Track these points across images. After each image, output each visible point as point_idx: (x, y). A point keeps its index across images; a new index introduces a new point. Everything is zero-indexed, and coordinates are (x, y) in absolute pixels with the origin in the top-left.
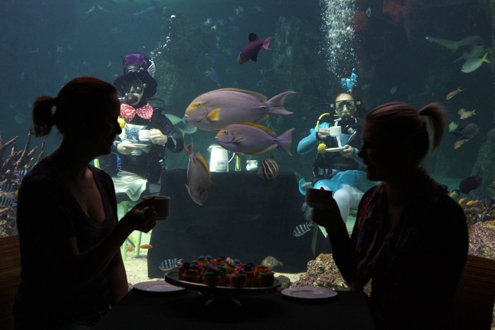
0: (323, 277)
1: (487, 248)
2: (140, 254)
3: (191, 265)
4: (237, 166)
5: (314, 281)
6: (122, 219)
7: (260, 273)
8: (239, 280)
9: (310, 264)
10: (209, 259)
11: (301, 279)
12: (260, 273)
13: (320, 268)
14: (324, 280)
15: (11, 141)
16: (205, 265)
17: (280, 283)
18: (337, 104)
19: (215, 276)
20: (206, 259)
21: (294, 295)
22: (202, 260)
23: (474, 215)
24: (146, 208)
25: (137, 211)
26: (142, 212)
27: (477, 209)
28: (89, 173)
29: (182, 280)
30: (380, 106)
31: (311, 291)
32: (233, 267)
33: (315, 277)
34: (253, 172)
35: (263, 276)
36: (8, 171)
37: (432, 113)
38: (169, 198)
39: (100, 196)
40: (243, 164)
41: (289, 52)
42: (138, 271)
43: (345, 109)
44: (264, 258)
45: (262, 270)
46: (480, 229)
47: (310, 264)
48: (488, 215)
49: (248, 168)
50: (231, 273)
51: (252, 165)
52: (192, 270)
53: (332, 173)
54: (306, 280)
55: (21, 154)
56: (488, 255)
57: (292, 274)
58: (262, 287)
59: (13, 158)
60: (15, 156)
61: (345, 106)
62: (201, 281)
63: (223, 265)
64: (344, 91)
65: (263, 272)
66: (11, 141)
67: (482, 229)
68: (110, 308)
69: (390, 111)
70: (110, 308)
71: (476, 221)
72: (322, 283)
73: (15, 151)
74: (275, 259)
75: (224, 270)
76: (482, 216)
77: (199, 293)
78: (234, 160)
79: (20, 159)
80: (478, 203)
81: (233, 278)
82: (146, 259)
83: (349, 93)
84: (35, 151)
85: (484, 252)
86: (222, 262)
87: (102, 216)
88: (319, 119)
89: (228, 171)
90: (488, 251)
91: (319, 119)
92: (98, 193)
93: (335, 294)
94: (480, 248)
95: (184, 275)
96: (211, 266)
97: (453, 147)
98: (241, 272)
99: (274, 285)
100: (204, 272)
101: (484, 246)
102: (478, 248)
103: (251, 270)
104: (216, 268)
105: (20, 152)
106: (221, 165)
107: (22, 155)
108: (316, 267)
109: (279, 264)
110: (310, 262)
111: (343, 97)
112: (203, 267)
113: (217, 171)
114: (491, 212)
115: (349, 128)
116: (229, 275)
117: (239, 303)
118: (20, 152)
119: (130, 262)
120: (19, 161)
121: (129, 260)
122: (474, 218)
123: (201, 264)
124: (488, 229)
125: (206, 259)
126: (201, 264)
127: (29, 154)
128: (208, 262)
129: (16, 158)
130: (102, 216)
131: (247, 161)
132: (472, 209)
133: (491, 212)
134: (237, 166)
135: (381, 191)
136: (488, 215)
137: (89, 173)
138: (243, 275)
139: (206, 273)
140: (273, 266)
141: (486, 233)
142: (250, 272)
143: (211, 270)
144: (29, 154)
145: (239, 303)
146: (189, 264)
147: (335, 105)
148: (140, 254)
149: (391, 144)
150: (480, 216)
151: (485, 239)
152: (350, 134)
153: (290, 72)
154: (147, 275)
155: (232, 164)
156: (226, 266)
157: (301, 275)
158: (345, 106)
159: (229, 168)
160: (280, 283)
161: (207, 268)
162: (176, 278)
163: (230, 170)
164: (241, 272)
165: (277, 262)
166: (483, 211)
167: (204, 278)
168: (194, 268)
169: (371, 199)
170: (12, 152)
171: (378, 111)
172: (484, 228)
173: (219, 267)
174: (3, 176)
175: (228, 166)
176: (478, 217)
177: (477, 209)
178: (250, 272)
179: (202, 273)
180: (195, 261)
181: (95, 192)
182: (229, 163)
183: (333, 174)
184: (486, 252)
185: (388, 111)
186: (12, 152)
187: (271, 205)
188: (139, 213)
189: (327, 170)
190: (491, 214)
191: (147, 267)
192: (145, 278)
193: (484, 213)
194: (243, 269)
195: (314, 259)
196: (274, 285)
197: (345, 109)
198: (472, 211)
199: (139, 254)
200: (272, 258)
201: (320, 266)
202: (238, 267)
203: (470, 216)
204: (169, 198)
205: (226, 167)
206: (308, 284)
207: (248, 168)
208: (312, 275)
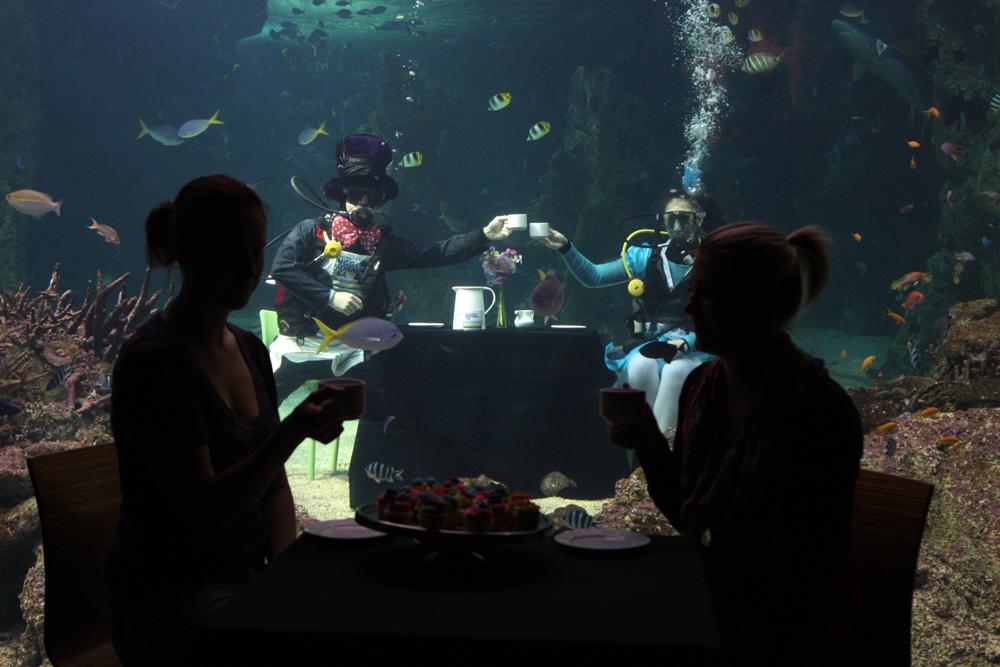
0: (641, 508)
1: (919, 457)
2: (338, 468)
3: (400, 494)
4: (500, 319)
5: (625, 514)
6: (287, 419)
7: (517, 507)
8: (478, 520)
9: (620, 486)
10: (430, 484)
11: (605, 510)
12: (517, 507)
13: (636, 491)
14: (643, 512)
15: (117, 281)
16: (423, 493)
17: (550, 523)
18: (666, 216)
19: (437, 514)
20: (425, 483)
21: (578, 544)
22: (417, 485)
23: (896, 401)
24: (327, 402)
25: (312, 406)
26: (319, 408)
27: (903, 391)
28: (230, 338)
29: (383, 520)
30: (721, 228)
31: (603, 536)
32: (470, 497)
33: (606, 512)
34: (526, 328)
35: (520, 512)
36: (113, 332)
37: (806, 243)
38: (363, 382)
39: (250, 377)
40: (510, 317)
41: (591, 125)
42: (332, 496)
43: (677, 226)
44: (545, 474)
45: (520, 501)
46: (907, 425)
47: (620, 486)
48: (920, 400)
49: (518, 322)
50: (466, 506)
51: (524, 318)
52: (398, 503)
53: (656, 329)
54: (612, 512)
55: (134, 302)
56: (920, 469)
57: (592, 502)
58: (519, 530)
59: (120, 310)
60: (123, 307)
61: (676, 221)
62: (414, 521)
63: (454, 494)
64: (681, 192)
65: (521, 505)
66: (117, 281)
67: (911, 424)
68: (266, 562)
69: (744, 234)
70: (266, 562)
71: (900, 411)
72: (640, 517)
73: (123, 298)
74: (563, 476)
75: (454, 503)
76: (911, 402)
77: (416, 541)
78: (495, 308)
79: (133, 311)
80: (904, 380)
81: (469, 517)
82: (347, 477)
83: (688, 197)
84: (158, 297)
85: (913, 464)
86: (454, 488)
87: (254, 409)
88: (628, 239)
89: (483, 328)
90: (919, 462)
91: (628, 239)
92: (247, 370)
93: (646, 541)
94: (906, 456)
95: (386, 511)
96: (433, 495)
97: (890, 284)
98: (482, 506)
99: (541, 527)
100: (421, 505)
101: (913, 454)
102: (902, 457)
103: (500, 502)
104: (441, 499)
105: (132, 299)
106: (472, 319)
107: (137, 305)
108: (629, 490)
109: (570, 485)
110: (620, 481)
111: (676, 206)
112: (420, 496)
113: (465, 329)
114: (925, 395)
115: (685, 255)
116: (462, 511)
117: (480, 556)
118: (132, 299)
119: (320, 483)
120: (131, 314)
121: (319, 479)
122: (897, 406)
123: (416, 491)
124: (920, 425)
125: (425, 483)
126: (416, 491)
127: (148, 302)
128: (429, 488)
129: (126, 309)
130: (254, 409)
131: (516, 312)
132: (893, 390)
133: (925, 395)
134: (500, 319)
135: (715, 376)
136: (920, 400)
137: (230, 338)
138: (485, 510)
139: (424, 507)
140: (560, 488)
141: (916, 431)
142: (498, 506)
143: (432, 503)
144: (148, 302)
145: (480, 556)
146: (395, 493)
147: (661, 217)
148: (338, 468)
149: (740, 294)
150: (907, 402)
151: (914, 441)
152: (686, 263)
153: (594, 160)
154: (348, 504)
155: (491, 317)
156: (458, 496)
157: (606, 504)
158: (676, 221)
159: (487, 321)
160: (550, 523)
161: (426, 500)
162: (373, 517)
163: (487, 327)
164: (482, 506)
165: (568, 481)
166: (912, 394)
167: (419, 516)
168: (402, 499)
169: (698, 390)
170: (120, 299)
171: (721, 235)
172: (913, 423)
173: (446, 498)
174: (105, 340)
175: (484, 320)
176: (904, 403)
177: (903, 391)
178: (498, 506)
179: (416, 507)
180: (406, 487)
181: (242, 368)
182: (486, 316)
183: (658, 331)
184: (916, 463)
185: (739, 235)
186: (120, 299)
187: (552, 393)
188: (315, 410)
189: (648, 324)
190: (925, 399)
191: (348, 491)
192: (345, 508)
193: (914, 397)
194: (485, 501)
195: (627, 476)
196: (541, 527)
197: (677, 226)
198: (894, 394)
199: (335, 467)
200: (558, 474)
201: (637, 489)
202: (479, 497)
203: (891, 402)
204: (363, 382)
205: (481, 322)
206: (615, 519)
207: (518, 322)
208: (624, 504)
